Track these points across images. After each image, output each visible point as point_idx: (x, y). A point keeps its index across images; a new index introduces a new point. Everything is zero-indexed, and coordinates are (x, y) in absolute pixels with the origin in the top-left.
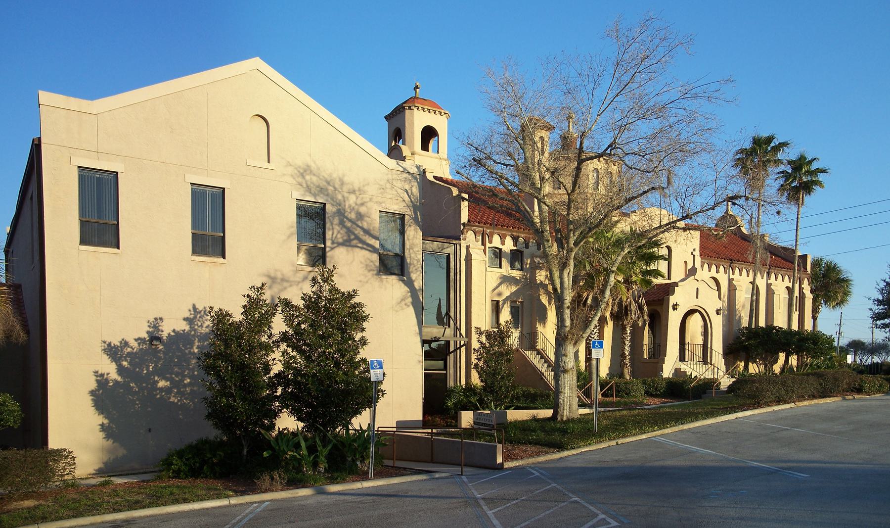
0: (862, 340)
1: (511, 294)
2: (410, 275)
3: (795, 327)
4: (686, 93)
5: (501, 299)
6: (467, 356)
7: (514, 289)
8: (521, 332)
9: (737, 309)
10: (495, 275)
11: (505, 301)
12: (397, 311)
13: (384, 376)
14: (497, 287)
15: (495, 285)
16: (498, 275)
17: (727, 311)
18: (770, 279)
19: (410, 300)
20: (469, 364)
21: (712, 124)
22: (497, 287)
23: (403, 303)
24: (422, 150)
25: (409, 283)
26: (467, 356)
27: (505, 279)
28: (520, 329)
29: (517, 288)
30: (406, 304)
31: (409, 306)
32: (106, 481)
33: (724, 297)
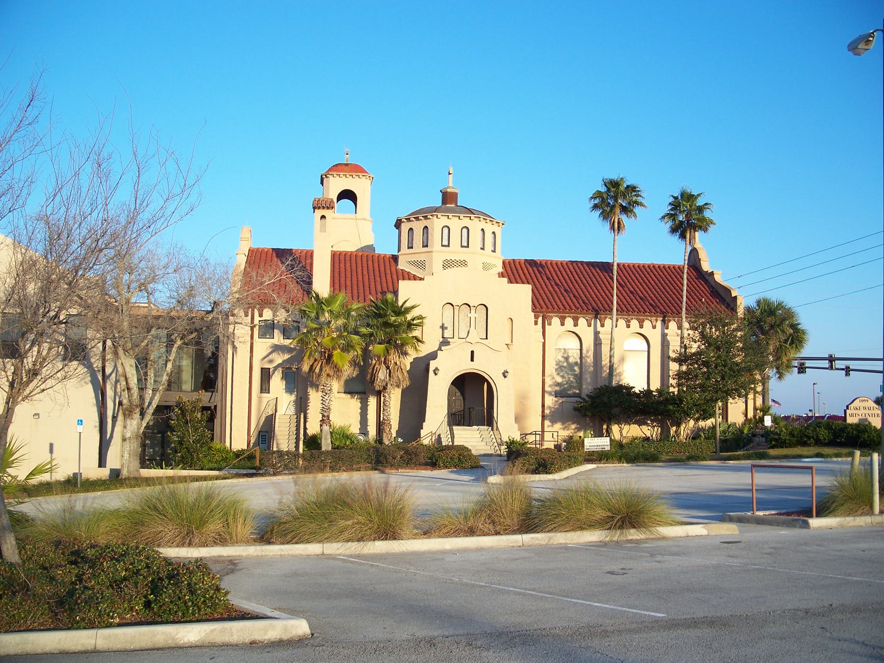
0: (466, 445)
1: (284, 361)
2: (90, 359)
3: (879, 366)
4: (167, 226)
5: (271, 366)
6: (663, 370)
7: (287, 356)
8: (297, 396)
9: (605, 366)
10: (262, 346)
11: (276, 368)
12: (77, 388)
13: (51, 451)
14: (268, 356)
15: (265, 354)
16: (268, 344)
17: (593, 367)
18: (667, 328)
19: (89, 378)
20: (665, 376)
21: (179, 246)
22: (268, 356)
23: (83, 381)
24: (251, 251)
25: (90, 367)
26: (663, 370)
27: (276, 348)
28: (295, 393)
29: (290, 356)
30: (85, 382)
31: (87, 384)
32: (647, 439)
33: (587, 352)
